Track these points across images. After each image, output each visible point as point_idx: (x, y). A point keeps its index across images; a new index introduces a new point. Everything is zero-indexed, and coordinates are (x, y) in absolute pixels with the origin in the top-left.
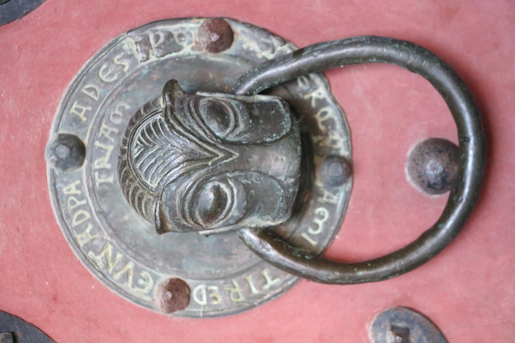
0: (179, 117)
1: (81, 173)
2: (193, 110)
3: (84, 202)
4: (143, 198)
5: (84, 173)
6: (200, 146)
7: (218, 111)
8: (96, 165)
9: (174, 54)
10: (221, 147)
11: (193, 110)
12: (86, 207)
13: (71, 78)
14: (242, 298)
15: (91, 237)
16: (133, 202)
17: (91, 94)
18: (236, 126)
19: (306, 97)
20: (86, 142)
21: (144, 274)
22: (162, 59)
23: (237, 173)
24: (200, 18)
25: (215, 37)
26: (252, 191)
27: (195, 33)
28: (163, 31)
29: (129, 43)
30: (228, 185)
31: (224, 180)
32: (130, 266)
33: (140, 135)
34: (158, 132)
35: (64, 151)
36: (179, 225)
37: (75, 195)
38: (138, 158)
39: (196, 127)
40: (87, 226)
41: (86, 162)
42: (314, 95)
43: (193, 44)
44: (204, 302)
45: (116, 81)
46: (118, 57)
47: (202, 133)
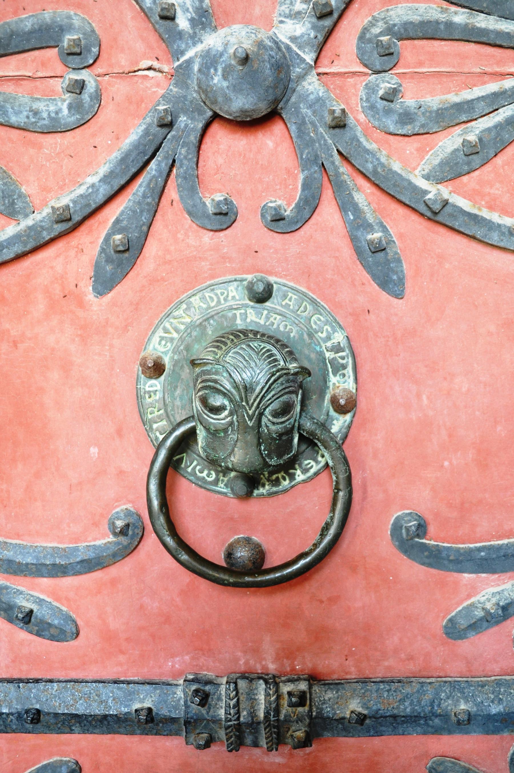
0: (281, 379)
1: (244, 299)
2: (287, 390)
3: (222, 302)
4: (218, 349)
5: (244, 302)
6: (257, 396)
7: (286, 409)
8: (249, 311)
9: (330, 370)
10: (257, 412)
11: (287, 390)
12: (219, 302)
13: (314, 294)
14: (150, 416)
15: (196, 307)
16: (217, 341)
17: (302, 309)
18: (274, 423)
19: (297, 466)
20: (268, 304)
21: (169, 344)
22: (327, 361)
23: (236, 423)
24: (356, 389)
25: (342, 402)
26: (222, 434)
27: (346, 386)
28: (347, 362)
29: (339, 337)
30: (227, 417)
31: (231, 414)
32: (175, 335)
33: (268, 348)
34: (270, 363)
35: (260, 287)
36: (198, 376)
37: (227, 296)
38: (249, 346)
39: (273, 393)
40: (204, 304)
41: (252, 304)
42: (298, 472)
43: (337, 385)
44: (147, 389)
45: (311, 327)
46: (329, 329)
47: (268, 398)
